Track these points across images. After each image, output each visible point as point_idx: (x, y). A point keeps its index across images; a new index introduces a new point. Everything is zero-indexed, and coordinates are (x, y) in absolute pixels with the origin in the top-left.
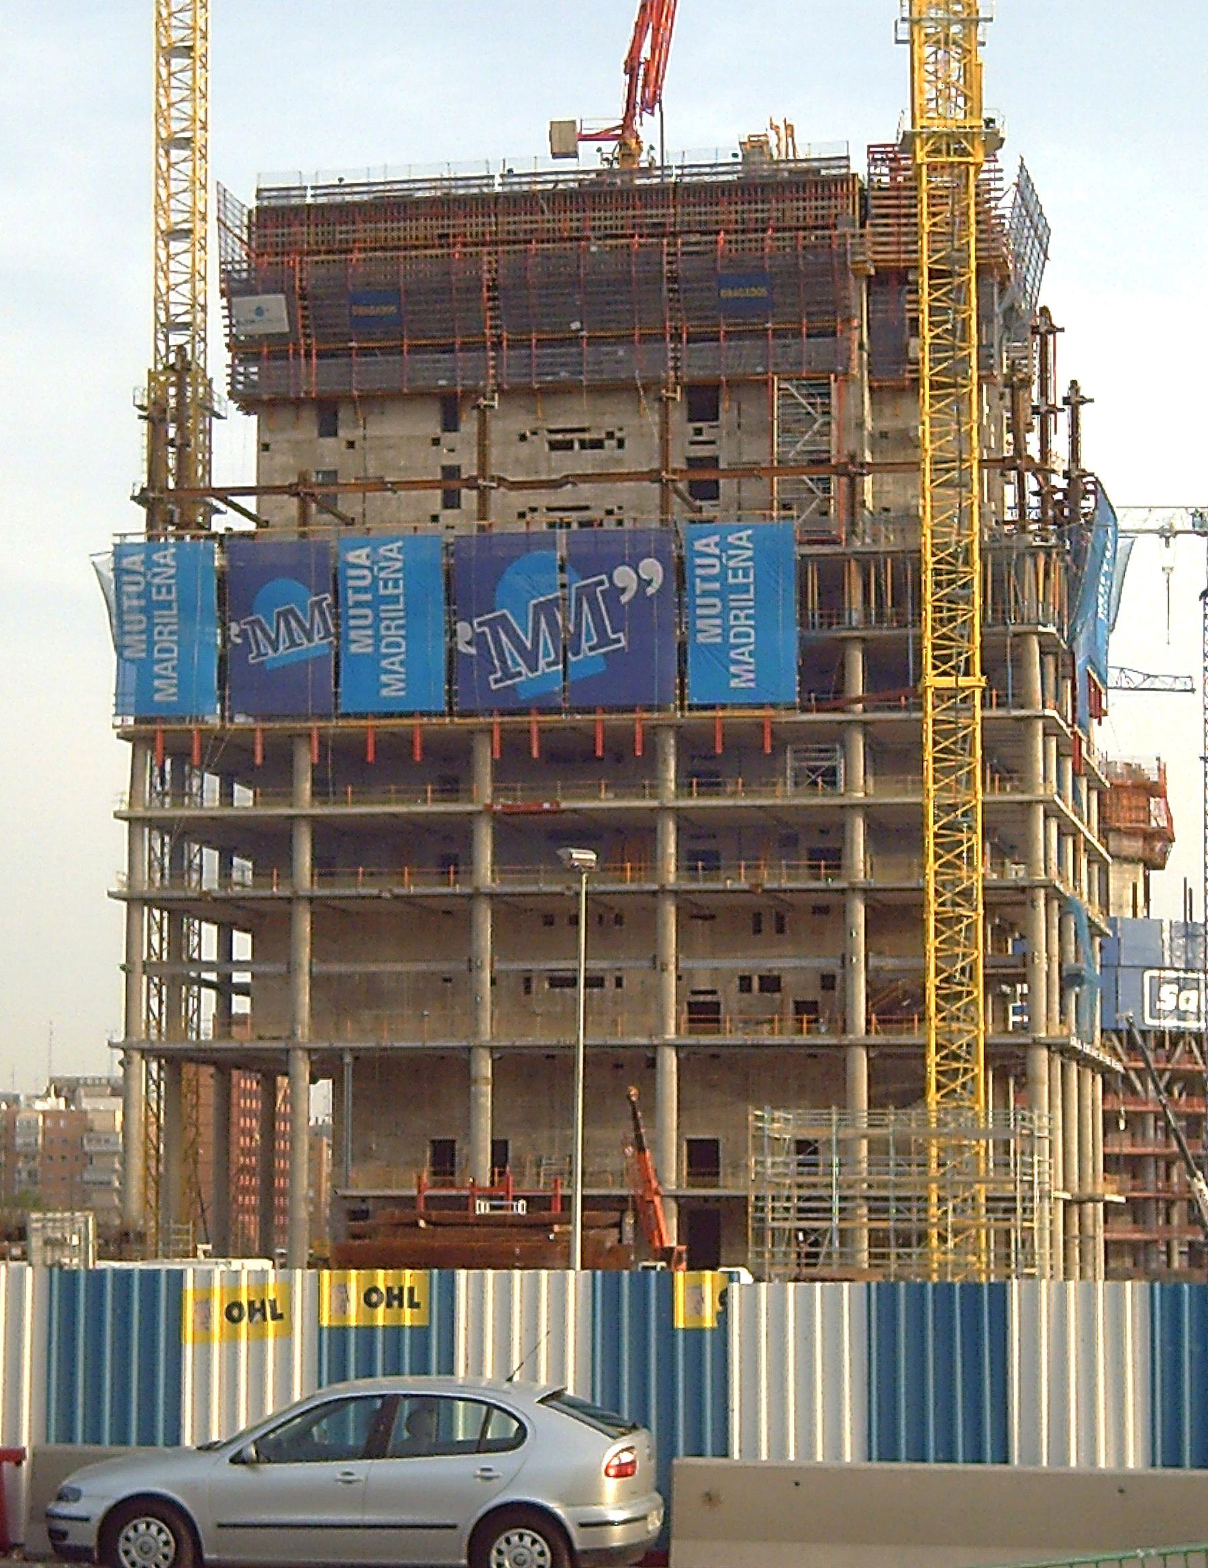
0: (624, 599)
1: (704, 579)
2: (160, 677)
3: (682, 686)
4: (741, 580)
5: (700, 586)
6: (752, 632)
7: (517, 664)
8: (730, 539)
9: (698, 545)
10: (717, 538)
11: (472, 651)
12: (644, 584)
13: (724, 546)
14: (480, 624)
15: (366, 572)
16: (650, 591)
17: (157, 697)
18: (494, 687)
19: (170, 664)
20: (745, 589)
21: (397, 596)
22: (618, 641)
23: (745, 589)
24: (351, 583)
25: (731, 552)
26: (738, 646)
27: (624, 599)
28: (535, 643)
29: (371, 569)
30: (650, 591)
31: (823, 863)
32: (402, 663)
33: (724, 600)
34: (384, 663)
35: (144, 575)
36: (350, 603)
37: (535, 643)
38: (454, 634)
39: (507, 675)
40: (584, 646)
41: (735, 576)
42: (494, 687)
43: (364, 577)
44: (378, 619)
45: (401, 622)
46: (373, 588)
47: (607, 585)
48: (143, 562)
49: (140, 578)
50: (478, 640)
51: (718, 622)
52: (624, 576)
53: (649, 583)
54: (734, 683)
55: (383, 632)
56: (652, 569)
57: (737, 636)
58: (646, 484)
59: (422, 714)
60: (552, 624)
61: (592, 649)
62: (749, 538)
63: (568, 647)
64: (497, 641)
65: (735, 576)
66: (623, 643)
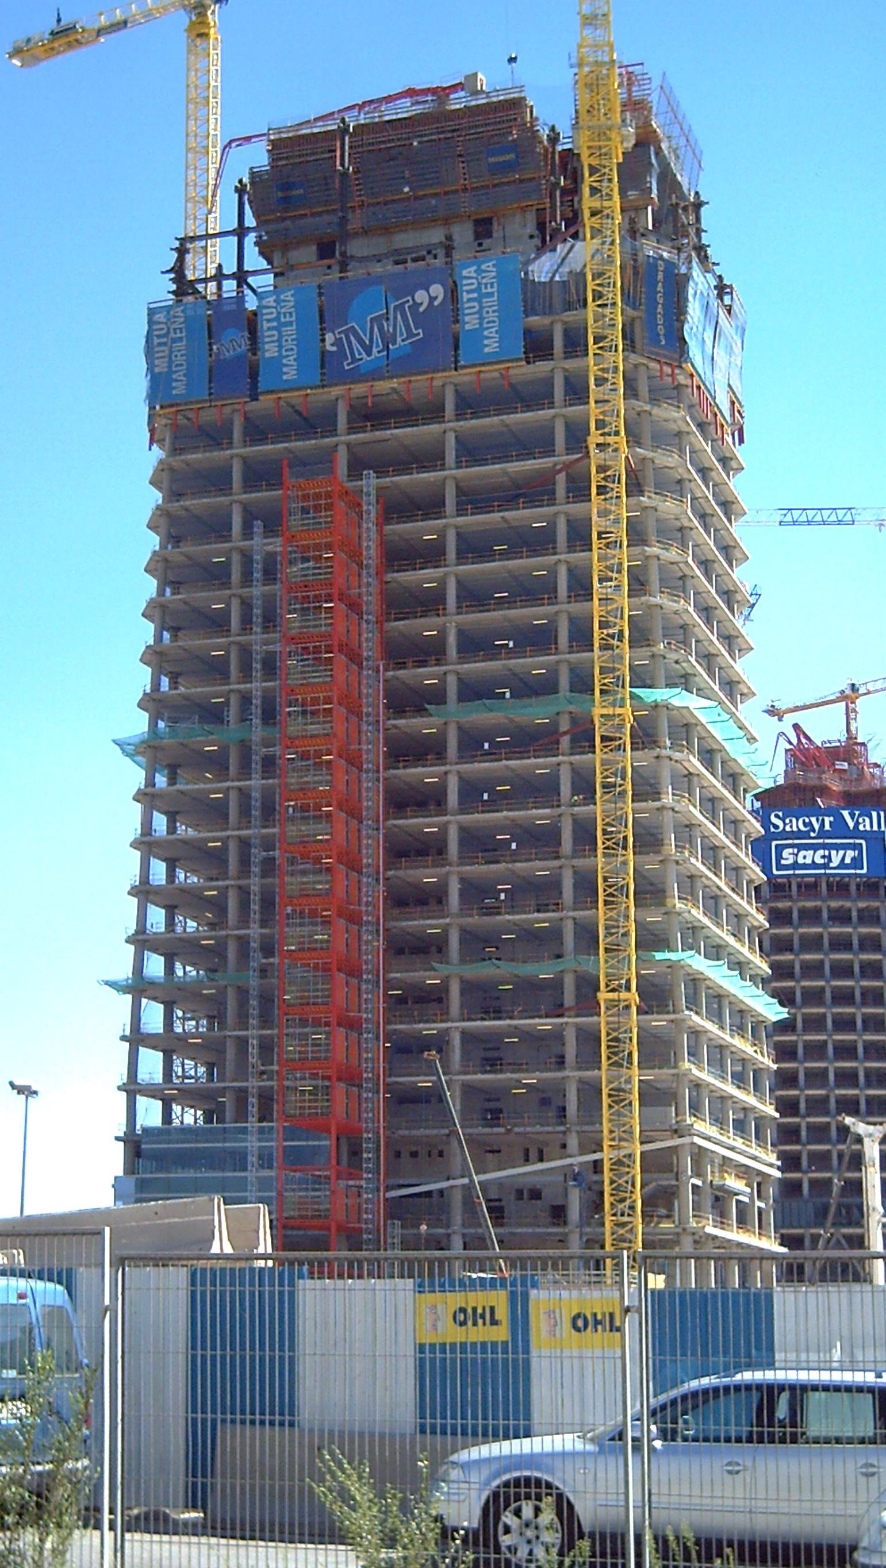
0: (421, 309)
1: (468, 292)
2: (287, 365)
3: (456, 356)
4: (288, 319)
5: (266, 325)
6: (496, 319)
7: (360, 354)
8: (282, 297)
9: (465, 273)
10: (475, 268)
11: (334, 349)
12: (432, 299)
13: (479, 271)
14: (339, 333)
15: (274, 310)
16: (436, 303)
17: (174, 392)
18: (347, 368)
19: (493, 330)
20: (290, 324)
21: (493, 293)
22: (418, 334)
23: (290, 324)
24: (465, 288)
25: (484, 275)
26: (488, 328)
27: (421, 309)
28: (371, 340)
29: (477, 279)
30: (436, 303)
31: (391, 469)
32: (295, 360)
33: (480, 303)
34: (284, 361)
35: (276, 308)
36: (465, 300)
37: (371, 340)
38: (323, 340)
39: (354, 360)
40: (399, 339)
41: (486, 288)
42: (347, 368)
43: (472, 284)
44: (481, 308)
45: (495, 308)
46: (277, 319)
47: (411, 302)
48: (475, 271)
49: (474, 281)
50: (338, 342)
51: (477, 316)
52: (421, 296)
53: (436, 298)
54: (486, 350)
55: (284, 344)
56: (437, 290)
57: (488, 322)
58: (250, 269)
59: (186, 404)
60: (381, 329)
61: (403, 340)
62: (494, 265)
63: (387, 340)
64: (350, 343)
65: (486, 288)
66: (421, 335)
